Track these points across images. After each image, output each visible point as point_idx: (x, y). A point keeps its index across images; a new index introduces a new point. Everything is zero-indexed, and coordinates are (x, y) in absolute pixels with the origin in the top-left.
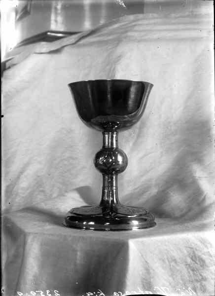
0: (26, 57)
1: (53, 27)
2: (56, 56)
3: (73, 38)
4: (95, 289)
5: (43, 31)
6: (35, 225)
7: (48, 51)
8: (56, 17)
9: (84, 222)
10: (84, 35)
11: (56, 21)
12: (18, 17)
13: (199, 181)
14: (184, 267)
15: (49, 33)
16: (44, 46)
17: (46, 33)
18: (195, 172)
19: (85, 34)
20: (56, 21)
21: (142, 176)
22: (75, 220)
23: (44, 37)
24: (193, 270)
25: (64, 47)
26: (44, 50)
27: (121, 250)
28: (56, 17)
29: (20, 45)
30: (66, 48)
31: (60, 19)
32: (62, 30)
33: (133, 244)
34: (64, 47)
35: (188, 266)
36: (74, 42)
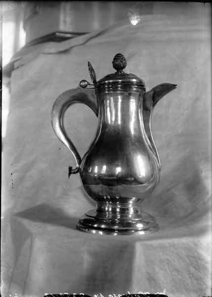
0: (36, 57)
1: (62, 28)
2: (64, 57)
3: (81, 39)
4: (102, 290)
5: (51, 31)
6: (36, 225)
7: (56, 52)
8: (65, 17)
9: (102, 225)
10: (92, 36)
11: (65, 22)
12: (27, 17)
13: (205, 181)
14: (187, 276)
15: (57, 34)
16: (52, 47)
17: (54, 34)
18: (202, 172)
19: (93, 34)
20: (65, 22)
21: (127, 159)
22: (86, 224)
23: (53, 38)
24: (196, 279)
25: (71, 48)
26: (53, 51)
27: (125, 253)
28: (65, 17)
29: (28, 45)
30: (74, 49)
31: (68, 19)
32: (71, 30)
33: (139, 248)
34: (71, 48)
35: (191, 275)
36: (82, 42)
